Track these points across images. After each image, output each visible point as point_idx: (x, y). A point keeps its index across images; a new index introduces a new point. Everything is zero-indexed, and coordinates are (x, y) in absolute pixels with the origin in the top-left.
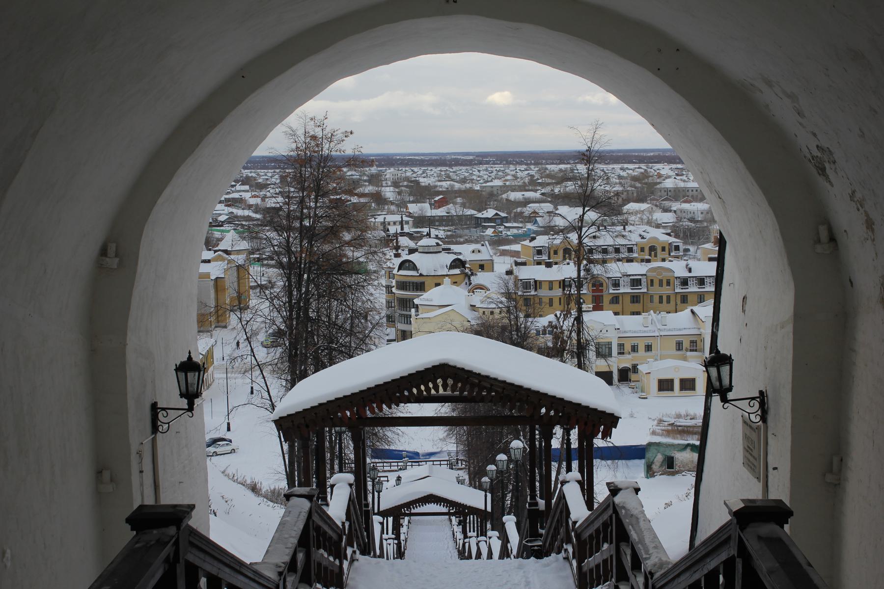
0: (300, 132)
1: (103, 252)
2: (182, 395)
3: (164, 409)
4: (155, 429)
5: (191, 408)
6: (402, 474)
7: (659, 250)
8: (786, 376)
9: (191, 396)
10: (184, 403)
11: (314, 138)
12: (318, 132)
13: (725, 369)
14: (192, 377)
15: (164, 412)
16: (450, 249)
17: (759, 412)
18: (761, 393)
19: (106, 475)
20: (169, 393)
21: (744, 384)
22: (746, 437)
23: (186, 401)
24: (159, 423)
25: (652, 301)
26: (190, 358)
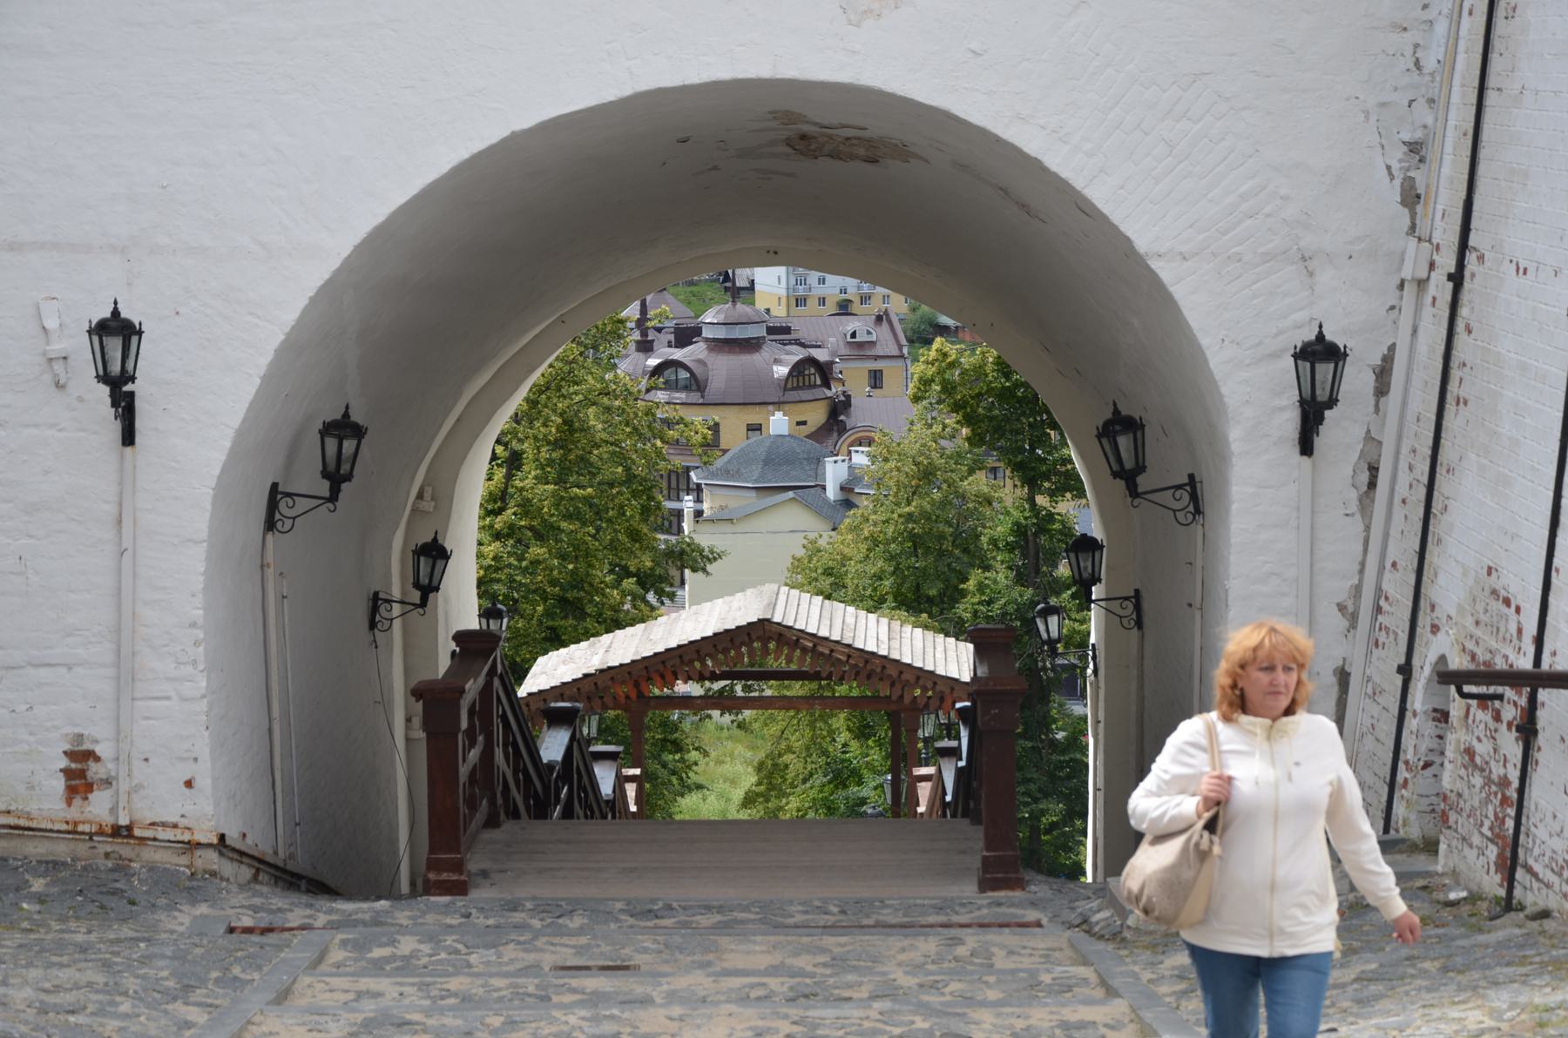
10: (324, 488)
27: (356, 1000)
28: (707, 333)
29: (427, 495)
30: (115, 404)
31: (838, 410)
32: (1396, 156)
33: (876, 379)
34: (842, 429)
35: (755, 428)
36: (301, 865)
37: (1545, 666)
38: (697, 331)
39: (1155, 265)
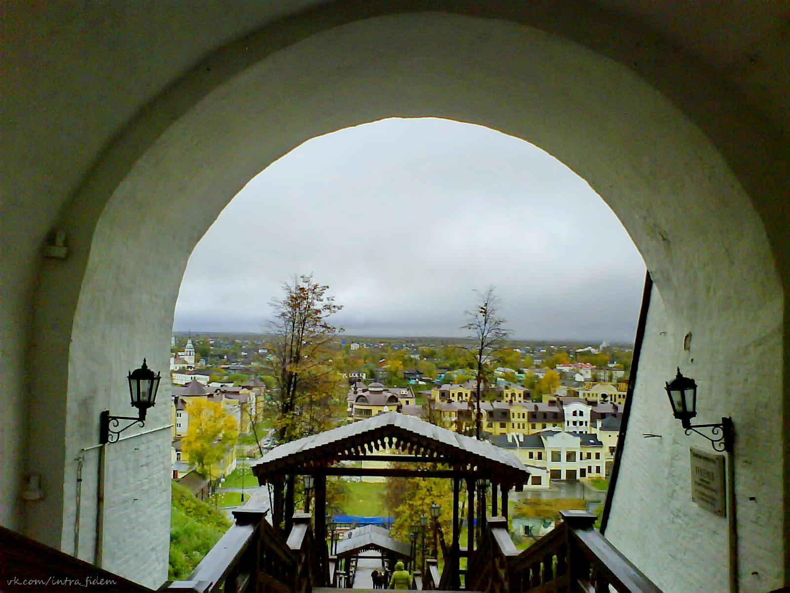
0: (293, 289)
1: (51, 239)
2: (133, 404)
3: (115, 418)
4: (104, 437)
5: (142, 418)
6: (353, 531)
7: (517, 396)
8: (773, 392)
9: (143, 405)
10: (135, 412)
11: (302, 289)
12: (306, 286)
13: (689, 393)
14: (145, 385)
15: (115, 421)
16: (388, 390)
17: (723, 441)
18: (724, 419)
19: (34, 482)
20: (121, 404)
21: (710, 407)
22: (697, 470)
23: (138, 410)
24: (110, 433)
25: (513, 427)
26: (144, 366)
29: (60, 240)
33: (407, 402)
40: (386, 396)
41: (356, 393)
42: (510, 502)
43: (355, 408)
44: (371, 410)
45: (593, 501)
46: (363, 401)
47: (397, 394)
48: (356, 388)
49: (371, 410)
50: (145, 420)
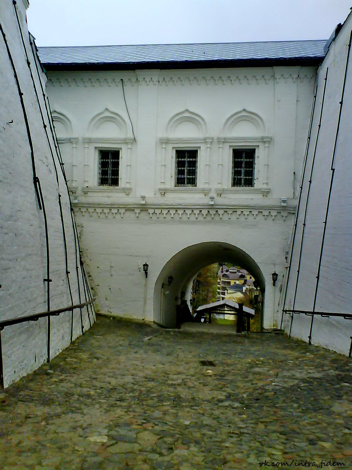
10: (168, 284)
27: (320, 439)
28: (230, 271)
30: (145, 273)
31: (246, 281)
32: (285, 253)
34: (246, 283)
35: (235, 283)
36: (164, 325)
37: (294, 310)
38: (229, 270)
39: (257, 264)
40: (238, 275)
41: (222, 272)
42: (46, 263)
43: (222, 281)
44: (230, 282)
45: (91, 267)
46: (226, 277)
47: (244, 273)
48: (222, 269)
49: (230, 282)
50: (340, 24)
